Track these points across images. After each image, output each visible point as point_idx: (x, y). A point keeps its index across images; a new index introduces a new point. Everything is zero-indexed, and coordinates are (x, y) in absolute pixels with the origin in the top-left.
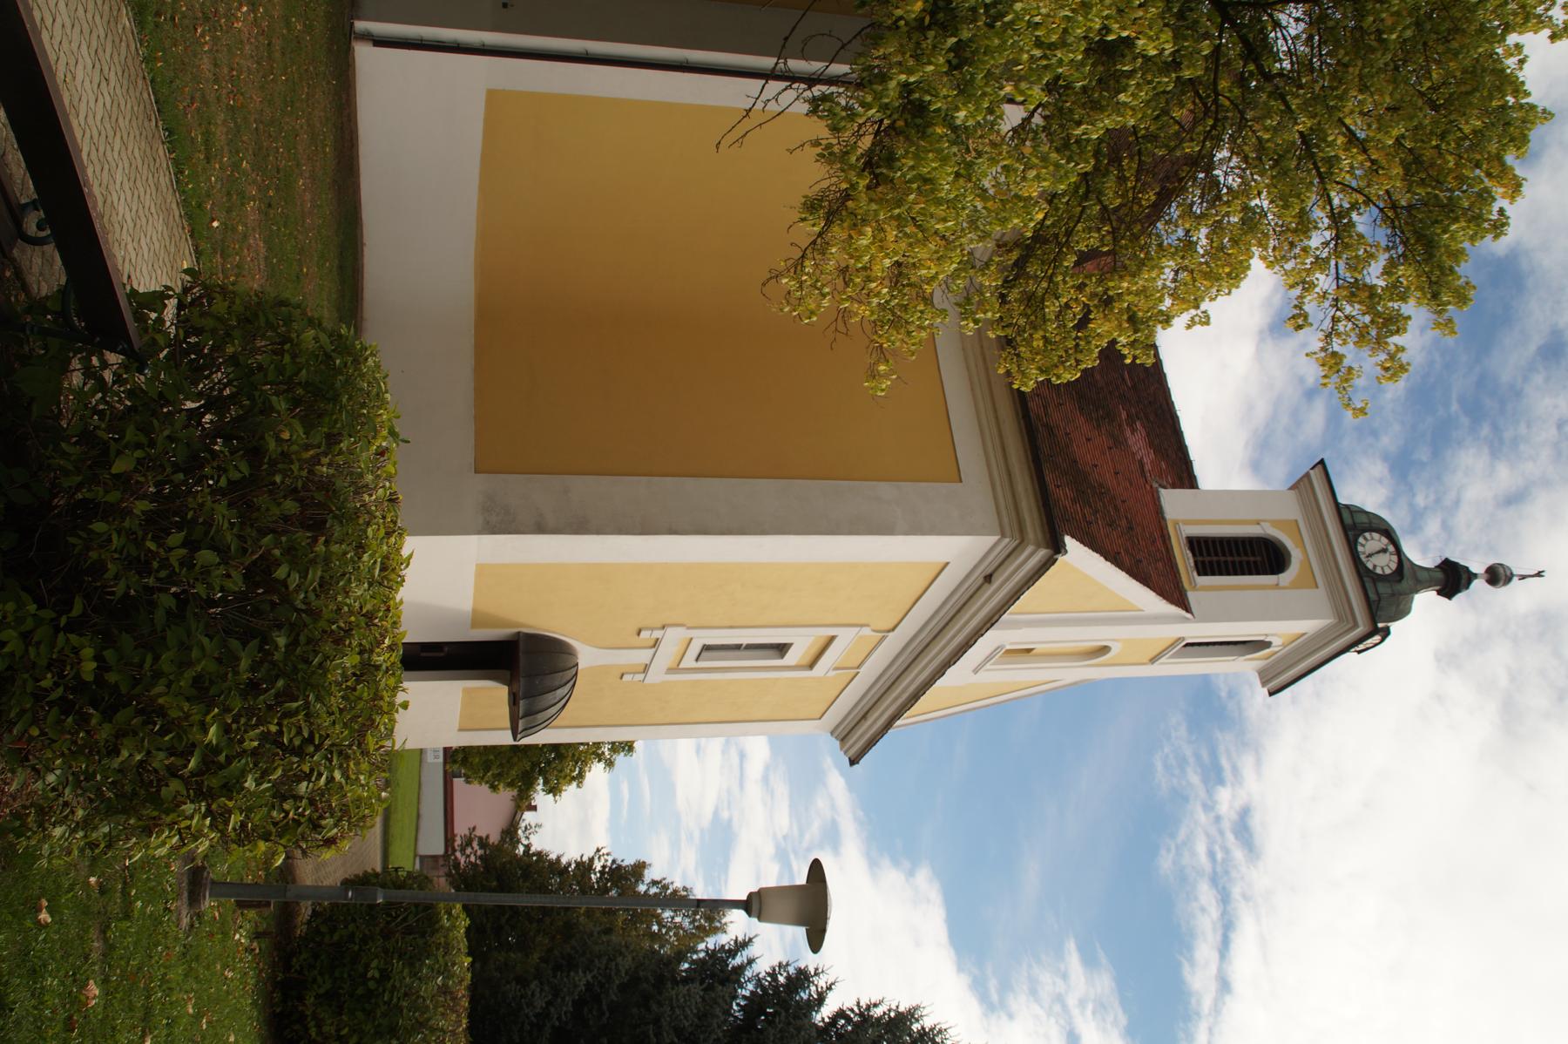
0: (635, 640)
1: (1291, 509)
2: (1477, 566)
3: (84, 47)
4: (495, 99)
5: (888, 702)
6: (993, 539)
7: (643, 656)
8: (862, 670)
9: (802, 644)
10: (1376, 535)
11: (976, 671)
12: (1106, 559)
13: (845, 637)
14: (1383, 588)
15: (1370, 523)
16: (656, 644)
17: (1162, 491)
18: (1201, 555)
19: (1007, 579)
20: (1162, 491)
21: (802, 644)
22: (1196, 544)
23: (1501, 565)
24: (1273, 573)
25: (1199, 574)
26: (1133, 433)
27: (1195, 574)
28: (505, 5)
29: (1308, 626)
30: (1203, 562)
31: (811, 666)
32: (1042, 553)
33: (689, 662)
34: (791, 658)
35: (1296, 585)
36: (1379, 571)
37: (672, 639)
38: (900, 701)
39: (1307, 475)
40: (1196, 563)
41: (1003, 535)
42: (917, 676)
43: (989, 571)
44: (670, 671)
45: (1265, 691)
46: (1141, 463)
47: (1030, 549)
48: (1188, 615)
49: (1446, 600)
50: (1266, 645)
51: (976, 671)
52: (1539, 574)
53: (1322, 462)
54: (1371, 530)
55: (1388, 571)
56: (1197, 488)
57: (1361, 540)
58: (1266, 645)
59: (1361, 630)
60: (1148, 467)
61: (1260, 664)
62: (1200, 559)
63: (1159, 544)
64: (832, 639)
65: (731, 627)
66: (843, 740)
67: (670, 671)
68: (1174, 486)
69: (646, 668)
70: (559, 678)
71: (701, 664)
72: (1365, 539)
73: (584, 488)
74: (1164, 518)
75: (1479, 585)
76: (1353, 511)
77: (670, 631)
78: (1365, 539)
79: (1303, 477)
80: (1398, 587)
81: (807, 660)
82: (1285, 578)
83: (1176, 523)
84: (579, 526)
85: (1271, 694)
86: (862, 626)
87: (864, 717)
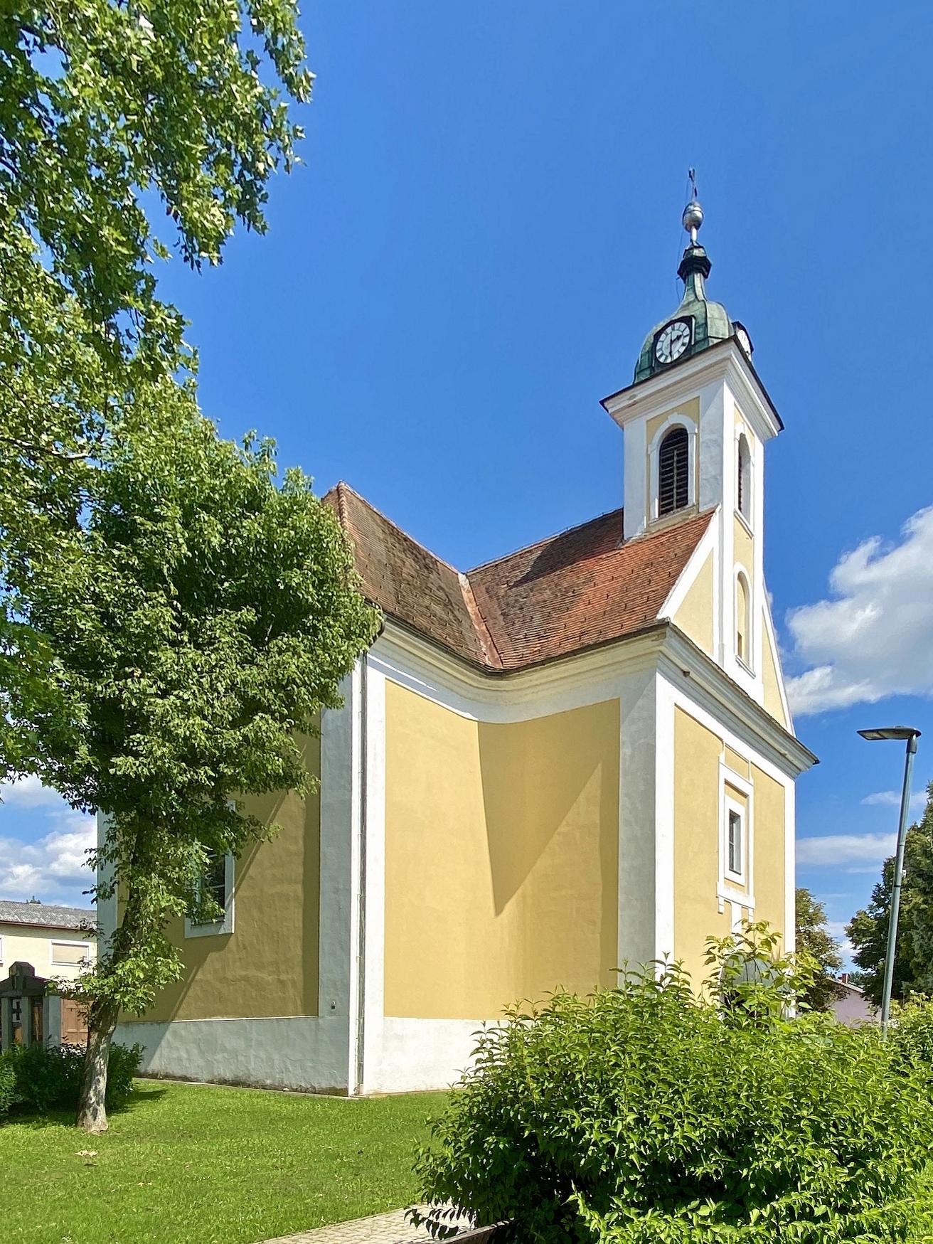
9: (730, 803)
11: (753, 676)
16: (727, 901)
21: (730, 803)
24: (686, 440)
29: (728, 398)
34: (740, 810)
35: (697, 420)
43: (681, 675)
50: (742, 436)
51: (753, 676)
64: (727, 782)
71: (743, 871)
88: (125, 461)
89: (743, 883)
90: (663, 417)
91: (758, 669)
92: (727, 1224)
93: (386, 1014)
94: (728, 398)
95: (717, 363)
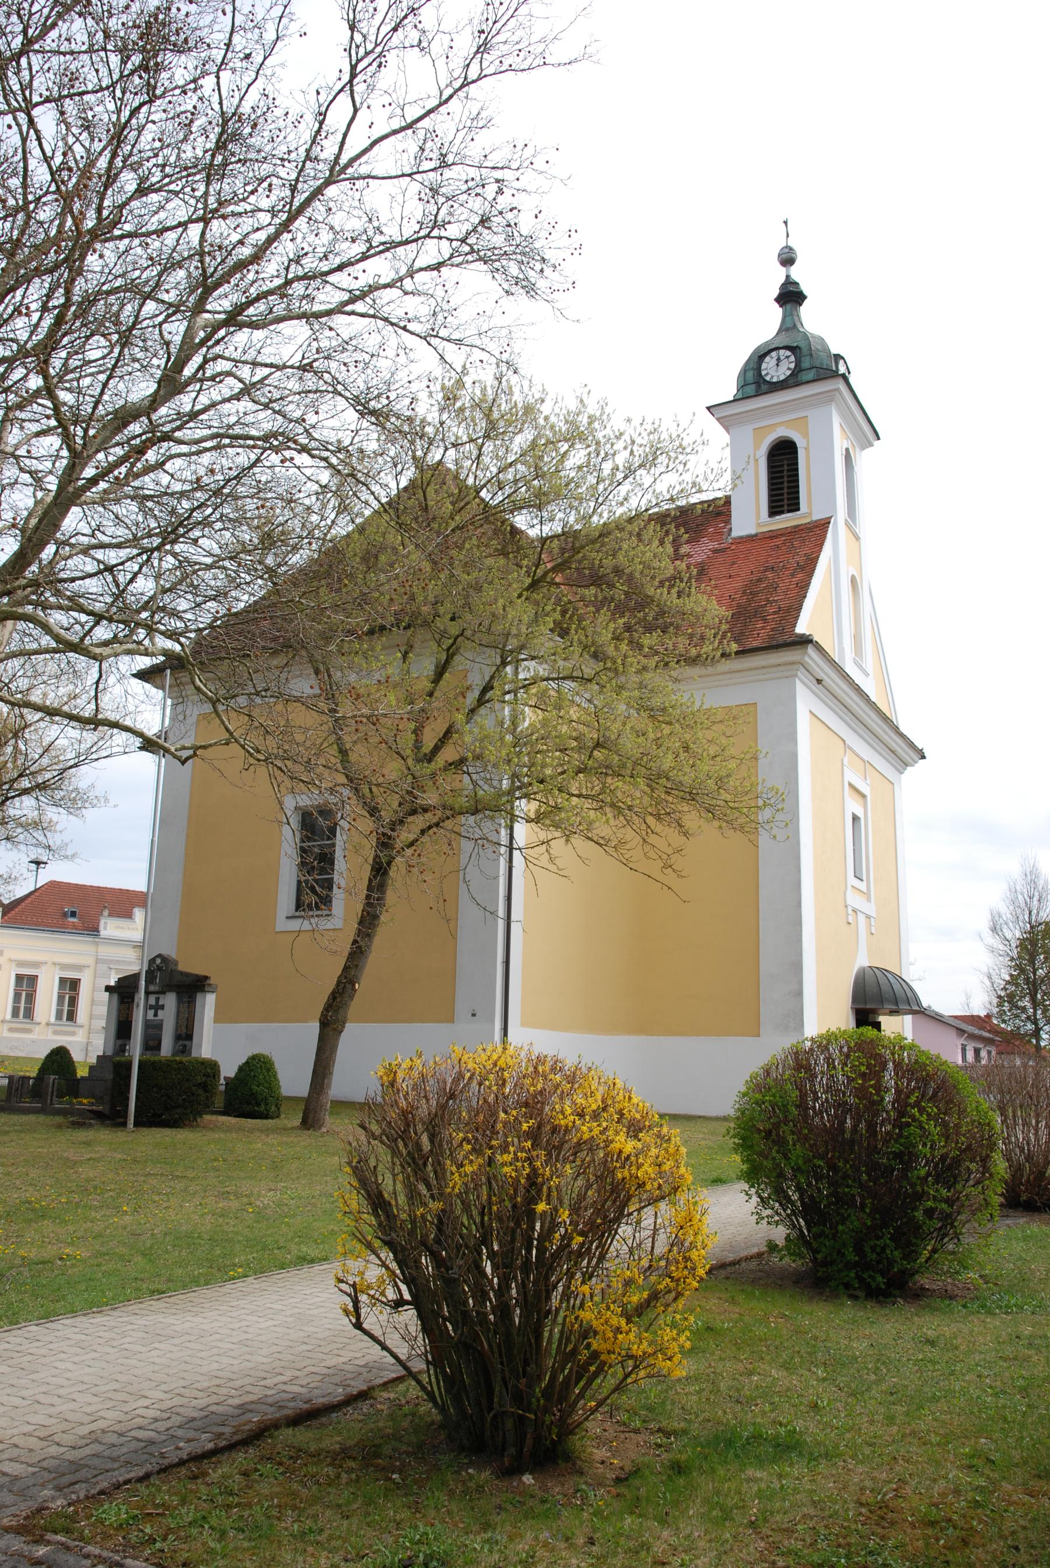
0: (853, 926)
1: (747, 432)
2: (779, 275)
3: (116, 1386)
4: (524, 1024)
5: (887, 738)
6: (798, 683)
7: (861, 918)
8: (866, 759)
9: (854, 806)
10: (764, 366)
11: (867, 675)
12: (805, 597)
13: (852, 776)
14: (806, 364)
15: (753, 369)
16: (855, 911)
17: (736, 533)
18: (782, 506)
19: (822, 670)
20: (736, 533)
21: (854, 806)
22: (775, 510)
23: (779, 255)
24: (796, 452)
25: (798, 509)
26: (691, 556)
27: (798, 513)
28: (474, 1015)
29: (836, 421)
30: (788, 505)
31: (864, 796)
32: (810, 649)
33: (862, 886)
34: (860, 813)
35: (806, 435)
36: (792, 366)
37: (855, 900)
38: (887, 729)
39: (718, 419)
40: (789, 511)
41: (796, 676)
42: (874, 721)
43: (815, 682)
44: (869, 900)
45: (876, 443)
46: (715, 551)
47: (807, 659)
48: (832, 521)
49: (806, 301)
50: (847, 450)
51: (867, 675)
52: (786, 223)
53: (708, 408)
54: (759, 369)
55: (792, 358)
56: (728, 501)
57: (768, 378)
58: (847, 450)
59: (841, 385)
60: (715, 545)
61: (857, 449)
62: (786, 508)
63: (778, 542)
64: (850, 785)
65: (845, 858)
66: (906, 764)
67: (869, 900)
68: (728, 521)
69: (868, 917)
70: (882, 981)
71: (864, 878)
72: (767, 374)
73: (769, 964)
74: (756, 535)
75: (796, 273)
76: (743, 383)
77: (849, 902)
78: (767, 374)
79: (721, 424)
80: (805, 350)
81: (860, 799)
82: (800, 444)
83: (759, 525)
84: (797, 967)
85: (879, 439)
86: (843, 765)
87: (893, 752)
88: (44, 309)
89: (864, 889)
90: (772, 427)
91: (869, 670)
92: (905, 1300)
93: (451, 1020)
94: (836, 421)
95: (828, 392)
